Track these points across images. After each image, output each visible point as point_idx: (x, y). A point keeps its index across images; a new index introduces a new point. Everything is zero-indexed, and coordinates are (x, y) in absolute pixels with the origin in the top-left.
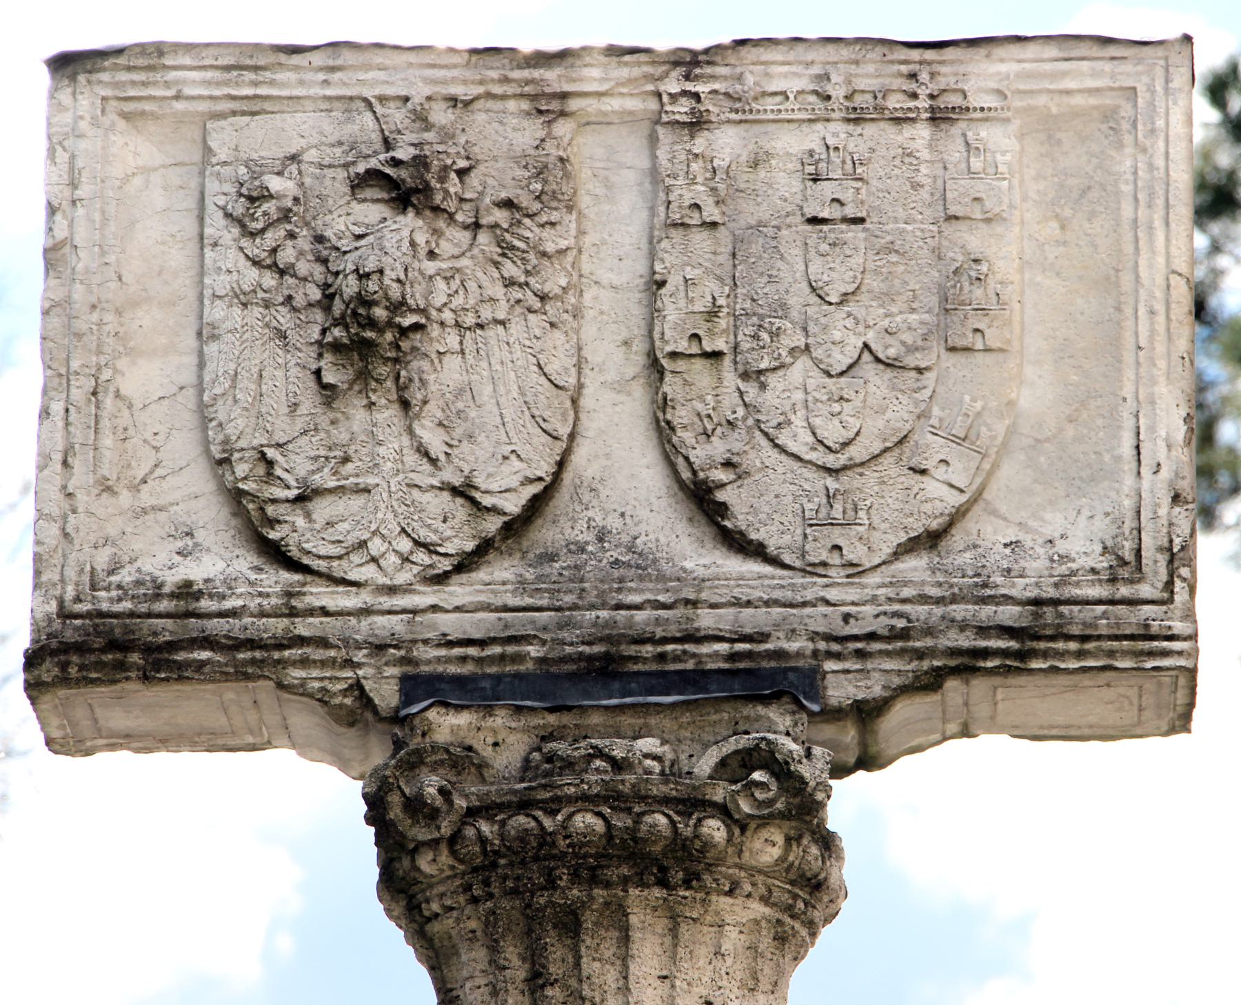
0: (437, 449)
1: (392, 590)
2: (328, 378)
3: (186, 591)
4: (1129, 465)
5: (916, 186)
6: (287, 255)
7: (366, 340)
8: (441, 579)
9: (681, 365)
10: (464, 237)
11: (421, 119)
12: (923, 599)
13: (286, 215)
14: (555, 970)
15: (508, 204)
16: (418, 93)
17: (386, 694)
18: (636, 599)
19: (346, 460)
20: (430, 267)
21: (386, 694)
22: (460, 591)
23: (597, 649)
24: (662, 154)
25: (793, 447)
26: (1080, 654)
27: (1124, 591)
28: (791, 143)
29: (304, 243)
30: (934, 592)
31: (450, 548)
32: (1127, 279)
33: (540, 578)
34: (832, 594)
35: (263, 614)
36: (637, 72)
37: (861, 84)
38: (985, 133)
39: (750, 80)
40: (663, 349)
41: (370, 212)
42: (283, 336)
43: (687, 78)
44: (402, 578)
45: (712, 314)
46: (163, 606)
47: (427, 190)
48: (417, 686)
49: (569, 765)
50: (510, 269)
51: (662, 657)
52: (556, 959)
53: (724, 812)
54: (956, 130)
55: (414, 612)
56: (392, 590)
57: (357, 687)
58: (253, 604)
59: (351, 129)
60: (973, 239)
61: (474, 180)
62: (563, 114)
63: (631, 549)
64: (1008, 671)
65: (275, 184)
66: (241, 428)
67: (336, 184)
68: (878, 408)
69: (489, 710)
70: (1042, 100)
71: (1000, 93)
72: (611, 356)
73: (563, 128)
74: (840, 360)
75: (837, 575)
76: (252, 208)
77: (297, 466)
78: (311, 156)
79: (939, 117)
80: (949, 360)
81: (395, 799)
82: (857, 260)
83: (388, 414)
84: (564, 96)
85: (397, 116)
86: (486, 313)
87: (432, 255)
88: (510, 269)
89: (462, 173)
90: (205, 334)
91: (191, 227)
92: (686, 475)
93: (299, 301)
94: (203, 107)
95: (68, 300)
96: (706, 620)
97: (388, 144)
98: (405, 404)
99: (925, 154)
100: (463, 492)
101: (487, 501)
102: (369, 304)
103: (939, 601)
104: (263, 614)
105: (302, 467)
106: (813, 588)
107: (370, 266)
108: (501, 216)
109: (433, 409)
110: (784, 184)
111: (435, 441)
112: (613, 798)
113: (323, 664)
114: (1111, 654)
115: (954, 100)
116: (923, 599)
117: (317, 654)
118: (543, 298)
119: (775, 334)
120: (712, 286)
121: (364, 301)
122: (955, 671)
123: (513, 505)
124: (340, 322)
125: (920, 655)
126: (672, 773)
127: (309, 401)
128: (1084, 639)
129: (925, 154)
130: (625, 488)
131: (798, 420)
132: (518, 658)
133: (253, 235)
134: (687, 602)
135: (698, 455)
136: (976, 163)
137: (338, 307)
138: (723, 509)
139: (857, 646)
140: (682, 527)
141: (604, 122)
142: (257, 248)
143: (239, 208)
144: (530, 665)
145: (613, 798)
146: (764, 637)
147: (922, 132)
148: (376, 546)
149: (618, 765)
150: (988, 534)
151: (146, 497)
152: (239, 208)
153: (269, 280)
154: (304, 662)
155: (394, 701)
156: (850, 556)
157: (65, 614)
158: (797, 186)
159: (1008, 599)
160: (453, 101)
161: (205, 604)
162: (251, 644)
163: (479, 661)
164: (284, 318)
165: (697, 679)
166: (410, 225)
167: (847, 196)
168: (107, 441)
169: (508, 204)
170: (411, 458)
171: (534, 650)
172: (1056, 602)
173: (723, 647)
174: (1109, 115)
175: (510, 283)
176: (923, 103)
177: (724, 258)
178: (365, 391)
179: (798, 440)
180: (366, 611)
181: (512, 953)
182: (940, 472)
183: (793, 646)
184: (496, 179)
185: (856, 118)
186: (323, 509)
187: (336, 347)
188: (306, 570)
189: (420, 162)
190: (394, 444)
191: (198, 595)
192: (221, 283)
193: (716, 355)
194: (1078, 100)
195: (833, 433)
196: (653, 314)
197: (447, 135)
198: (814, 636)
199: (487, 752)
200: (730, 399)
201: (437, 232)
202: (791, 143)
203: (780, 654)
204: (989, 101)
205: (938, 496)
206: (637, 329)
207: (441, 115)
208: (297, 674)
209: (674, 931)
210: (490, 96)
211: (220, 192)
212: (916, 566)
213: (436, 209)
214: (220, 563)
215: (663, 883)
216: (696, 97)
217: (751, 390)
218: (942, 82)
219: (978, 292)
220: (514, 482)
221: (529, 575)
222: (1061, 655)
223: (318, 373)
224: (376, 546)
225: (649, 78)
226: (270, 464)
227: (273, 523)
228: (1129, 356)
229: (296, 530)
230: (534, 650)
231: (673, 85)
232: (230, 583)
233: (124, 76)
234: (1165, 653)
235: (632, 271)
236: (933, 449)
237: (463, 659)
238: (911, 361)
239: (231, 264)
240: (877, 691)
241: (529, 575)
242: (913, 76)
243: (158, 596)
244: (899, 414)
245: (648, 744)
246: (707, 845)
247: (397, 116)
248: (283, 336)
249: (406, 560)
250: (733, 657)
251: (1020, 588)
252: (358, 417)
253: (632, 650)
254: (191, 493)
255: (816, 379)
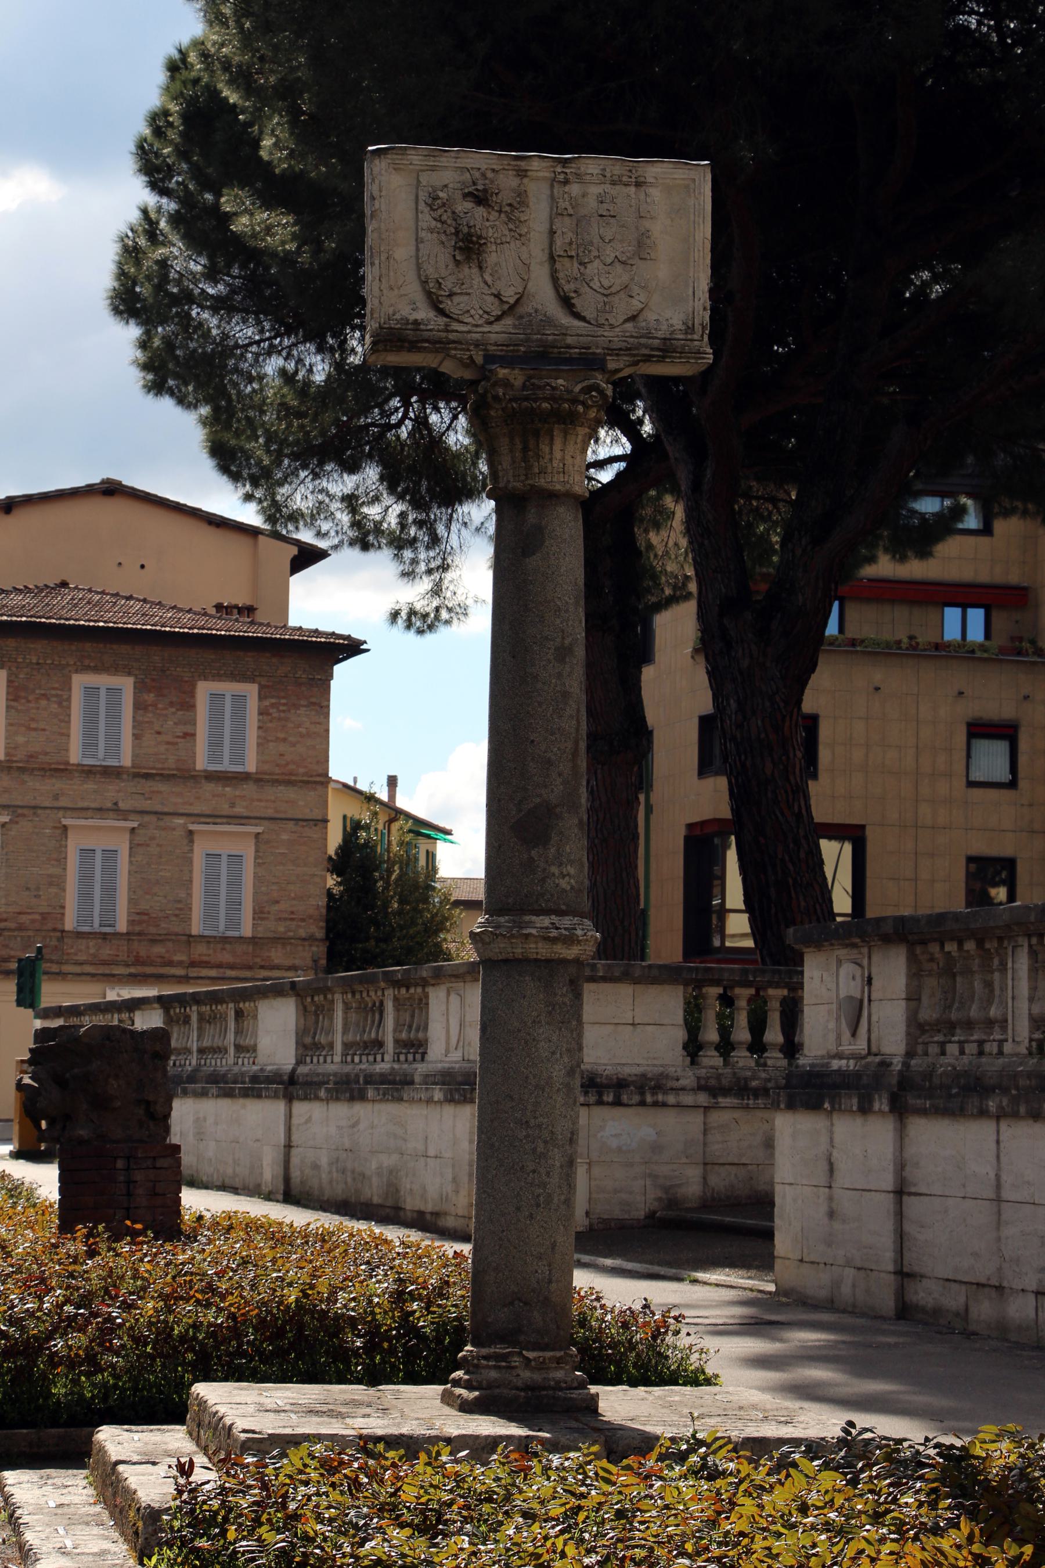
0: (490, 282)
1: (477, 326)
2: (458, 258)
3: (416, 322)
4: (691, 298)
5: (631, 206)
6: (444, 218)
7: (469, 247)
8: (491, 323)
9: (561, 259)
10: (497, 214)
11: (484, 175)
12: (632, 337)
13: (444, 205)
14: (531, 446)
15: (510, 205)
16: (484, 167)
17: (479, 360)
18: (548, 332)
19: (463, 284)
20: (488, 224)
21: (479, 360)
22: (496, 327)
23: (541, 349)
24: (555, 191)
25: (595, 287)
26: (680, 358)
27: (689, 337)
28: (595, 190)
29: (449, 214)
30: (635, 334)
31: (494, 314)
32: (691, 239)
33: (520, 324)
34: (606, 334)
35: (439, 331)
36: (548, 164)
37: (615, 172)
38: (652, 191)
39: (582, 169)
40: (556, 254)
41: (469, 205)
42: (443, 243)
43: (564, 167)
44: (480, 322)
45: (571, 243)
46: (410, 327)
47: (487, 200)
48: (489, 358)
49: (539, 388)
50: (511, 226)
51: (560, 353)
52: (532, 443)
53: (583, 403)
54: (642, 189)
55: (484, 333)
56: (477, 326)
57: (471, 357)
58: (436, 328)
59: (463, 178)
60: (647, 224)
61: (500, 196)
62: (526, 176)
63: (545, 315)
64: (658, 361)
65: (441, 194)
66: (431, 272)
67: (458, 195)
68: (618, 277)
69: (513, 369)
70: (668, 181)
71: (656, 178)
72: (537, 249)
73: (526, 181)
74: (609, 261)
75: (607, 328)
76: (434, 202)
77: (448, 285)
78: (451, 185)
79: (638, 185)
80: (640, 262)
81: (489, 395)
82: (614, 230)
83: (475, 270)
84: (526, 171)
85: (477, 174)
86: (504, 240)
87: (488, 220)
88: (511, 226)
89: (497, 194)
90: (418, 241)
91: (413, 206)
92: (562, 294)
93: (448, 232)
94: (418, 168)
95: (379, 228)
96: (569, 340)
97: (474, 184)
98: (480, 268)
99: (633, 196)
100: (498, 296)
101: (505, 299)
102: (472, 236)
103: (637, 337)
104: (439, 331)
105: (450, 286)
106: (600, 331)
107: (472, 224)
108: (508, 209)
109: (489, 270)
110: (592, 203)
111: (488, 278)
112: (553, 399)
113: (461, 350)
114: (689, 358)
115: (642, 179)
116: (632, 337)
117: (459, 347)
118: (520, 235)
119: (590, 251)
120: (570, 234)
121: (470, 235)
122: (645, 361)
123: (512, 301)
124: (462, 240)
125: (635, 355)
126: (569, 391)
127: (451, 266)
128: (681, 353)
129: (633, 196)
130: (543, 297)
131: (596, 279)
132: (518, 351)
133: (434, 210)
134: (564, 334)
135: (566, 288)
136: (648, 200)
137: (461, 236)
138: (573, 305)
139: (617, 352)
140: (560, 309)
141: (537, 179)
142: (436, 214)
143: (430, 201)
144: (520, 354)
145: (553, 399)
146: (589, 348)
147: (632, 189)
148: (473, 312)
149: (554, 388)
150: (651, 316)
151: (402, 292)
152: (430, 201)
153: (439, 225)
154: (455, 349)
155: (482, 362)
156: (611, 322)
157: (381, 327)
158: (596, 204)
159: (656, 338)
160: (493, 170)
161: (422, 327)
162: (440, 342)
163: (506, 351)
164: (443, 237)
165: (570, 361)
166: (481, 211)
167: (611, 208)
168: (392, 274)
169: (510, 205)
170: (482, 285)
171: (522, 349)
172: (670, 339)
173: (577, 350)
174: (687, 187)
175: (510, 230)
176: (633, 180)
177: (574, 226)
178: (469, 262)
179: (596, 285)
180: (469, 332)
181: (517, 441)
182: (637, 297)
183: (598, 351)
184: (506, 198)
185: (613, 183)
186: (456, 299)
187: (460, 248)
188: (451, 318)
189: (485, 191)
190: (477, 281)
191: (420, 324)
192: (425, 225)
193: (571, 257)
194: (678, 182)
195: (606, 283)
196: (551, 243)
197: (492, 182)
198: (603, 349)
199: (512, 381)
200: (576, 271)
201: (489, 213)
202: (595, 190)
203: (594, 353)
204: (652, 180)
205: (636, 304)
206: (546, 245)
207: (490, 175)
208: (453, 352)
209: (565, 438)
210: (504, 169)
211: (423, 196)
212: (629, 326)
213: (490, 206)
214: (424, 313)
215: (564, 423)
216: (566, 173)
217: (582, 268)
218: (639, 173)
219: (648, 241)
220: (512, 293)
221: (517, 323)
222: (675, 357)
223: (454, 256)
224: (473, 312)
225: (553, 167)
226: (440, 284)
227: (441, 302)
228: (692, 264)
229: (448, 305)
230: (522, 349)
231: (559, 169)
232: (429, 320)
233: (395, 157)
234: (704, 358)
235: (544, 227)
236: (636, 290)
237: (502, 350)
238: (630, 262)
239: (427, 219)
240: (622, 366)
241: (517, 323)
242: (630, 171)
243: (408, 324)
244: (625, 278)
245: (560, 381)
246: (579, 413)
247: (477, 174)
248: (443, 243)
249: (481, 316)
250: (580, 353)
251: (659, 334)
252: (466, 270)
253: (551, 350)
254: (414, 290)
255: (601, 266)
